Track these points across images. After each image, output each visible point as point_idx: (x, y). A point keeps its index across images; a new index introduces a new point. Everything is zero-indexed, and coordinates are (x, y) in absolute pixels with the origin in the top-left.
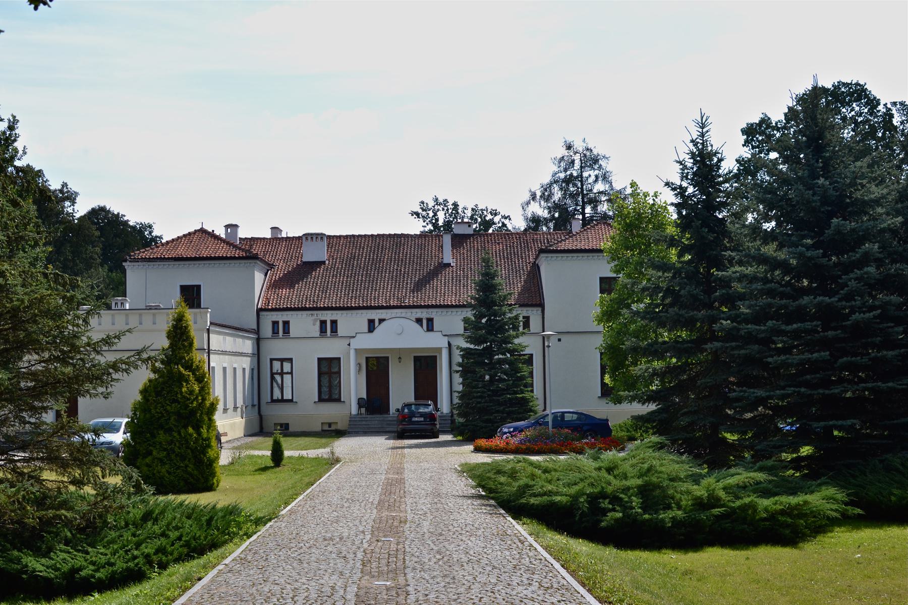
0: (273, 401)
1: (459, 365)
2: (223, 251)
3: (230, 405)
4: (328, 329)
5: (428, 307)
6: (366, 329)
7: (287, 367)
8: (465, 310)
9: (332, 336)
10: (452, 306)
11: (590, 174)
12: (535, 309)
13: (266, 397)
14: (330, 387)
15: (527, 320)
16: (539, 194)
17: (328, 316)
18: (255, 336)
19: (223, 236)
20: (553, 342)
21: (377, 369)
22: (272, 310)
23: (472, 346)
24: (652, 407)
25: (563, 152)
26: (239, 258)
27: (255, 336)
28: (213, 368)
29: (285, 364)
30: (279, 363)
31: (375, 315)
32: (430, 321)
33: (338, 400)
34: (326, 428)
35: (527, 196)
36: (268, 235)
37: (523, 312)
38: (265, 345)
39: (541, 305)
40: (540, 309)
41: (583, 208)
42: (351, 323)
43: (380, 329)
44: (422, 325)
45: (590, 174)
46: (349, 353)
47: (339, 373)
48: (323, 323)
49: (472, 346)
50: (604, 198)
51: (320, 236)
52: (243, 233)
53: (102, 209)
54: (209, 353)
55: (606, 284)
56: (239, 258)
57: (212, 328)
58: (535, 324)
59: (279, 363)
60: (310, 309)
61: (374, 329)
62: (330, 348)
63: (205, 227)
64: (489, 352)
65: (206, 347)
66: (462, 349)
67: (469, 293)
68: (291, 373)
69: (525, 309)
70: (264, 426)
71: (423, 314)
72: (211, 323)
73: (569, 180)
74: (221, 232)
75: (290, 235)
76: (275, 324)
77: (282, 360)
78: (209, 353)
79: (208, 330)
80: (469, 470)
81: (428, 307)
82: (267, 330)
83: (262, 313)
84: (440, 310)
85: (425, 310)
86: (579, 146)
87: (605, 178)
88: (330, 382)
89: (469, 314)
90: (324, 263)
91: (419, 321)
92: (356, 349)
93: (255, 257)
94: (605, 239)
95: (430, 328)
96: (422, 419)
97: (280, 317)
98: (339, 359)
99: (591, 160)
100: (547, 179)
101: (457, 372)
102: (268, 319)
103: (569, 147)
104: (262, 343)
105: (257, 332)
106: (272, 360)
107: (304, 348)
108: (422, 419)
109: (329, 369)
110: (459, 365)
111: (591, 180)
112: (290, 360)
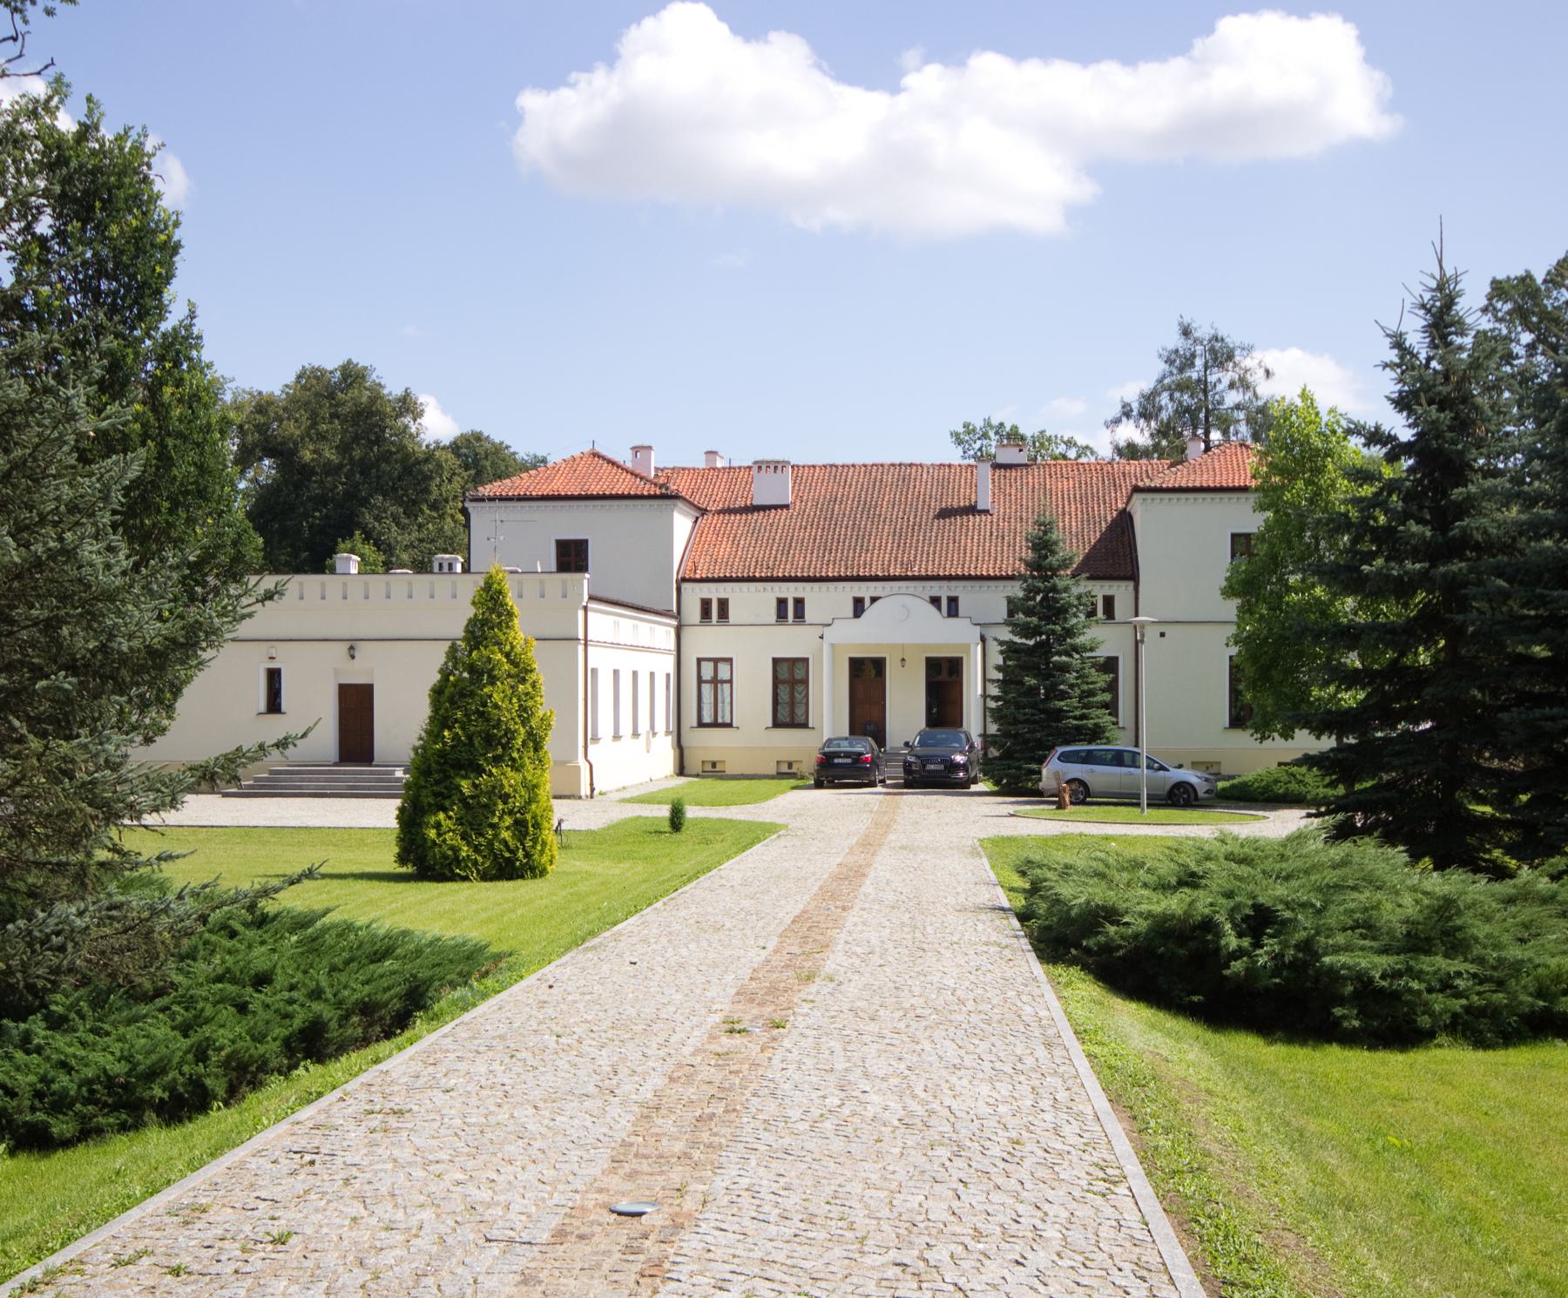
0: (701, 725)
1: (998, 668)
2: (624, 485)
3: (644, 726)
4: (790, 612)
5: (950, 578)
6: (850, 613)
7: (724, 672)
8: (1009, 583)
9: (795, 623)
10: (989, 578)
11: (1221, 378)
12: (1123, 584)
13: (690, 718)
14: (792, 704)
15: (1109, 602)
16: (1135, 406)
17: (790, 591)
18: (675, 623)
19: (629, 465)
20: (1151, 634)
21: (867, 676)
22: (701, 580)
23: (1017, 639)
24: (1328, 743)
25: (1175, 341)
26: (650, 497)
27: (675, 623)
28: (594, 671)
29: (721, 666)
30: (711, 664)
31: (865, 590)
32: (953, 601)
33: (805, 725)
34: (784, 769)
35: (1116, 411)
36: (701, 463)
37: (1100, 589)
38: (687, 633)
39: (1132, 575)
40: (1131, 584)
41: (1207, 433)
42: (826, 602)
43: (871, 612)
44: (939, 608)
45: (1221, 378)
46: (821, 650)
47: (805, 682)
48: (782, 603)
49: (1017, 639)
50: (1242, 415)
51: (777, 466)
52: (656, 460)
53: (478, 437)
54: (586, 645)
55: (1240, 542)
56: (650, 497)
57: (592, 605)
58: (1122, 608)
59: (711, 664)
60: (761, 580)
61: (863, 611)
62: (791, 642)
63: (599, 449)
64: (1044, 649)
65: (581, 636)
66: (1001, 643)
67: (1015, 556)
68: (730, 681)
69: (1106, 584)
70: (686, 764)
71: (943, 590)
72: (591, 598)
73: (1182, 387)
74: (624, 457)
75: (735, 464)
76: (706, 605)
77: (716, 661)
78: (586, 645)
79: (585, 608)
80: (996, 847)
81: (950, 578)
82: (693, 612)
83: (685, 586)
84: (968, 584)
85: (945, 584)
86: (1203, 331)
87: (1242, 384)
88: (792, 696)
89: (1016, 590)
90: (787, 507)
91: (935, 601)
92: (833, 645)
93: (676, 497)
94: (1245, 466)
95: (953, 608)
96: (849, 761)
97: (714, 592)
98: (806, 660)
99: (1221, 355)
100: (1147, 385)
101: (993, 681)
102: (694, 595)
103: (1186, 332)
104: (686, 632)
105: (678, 615)
106: (699, 661)
107: (751, 645)
108: (849, 761)
109: (790, 679)
110: (998, 668)
111: (1219, 387)
112: (729, 660)
